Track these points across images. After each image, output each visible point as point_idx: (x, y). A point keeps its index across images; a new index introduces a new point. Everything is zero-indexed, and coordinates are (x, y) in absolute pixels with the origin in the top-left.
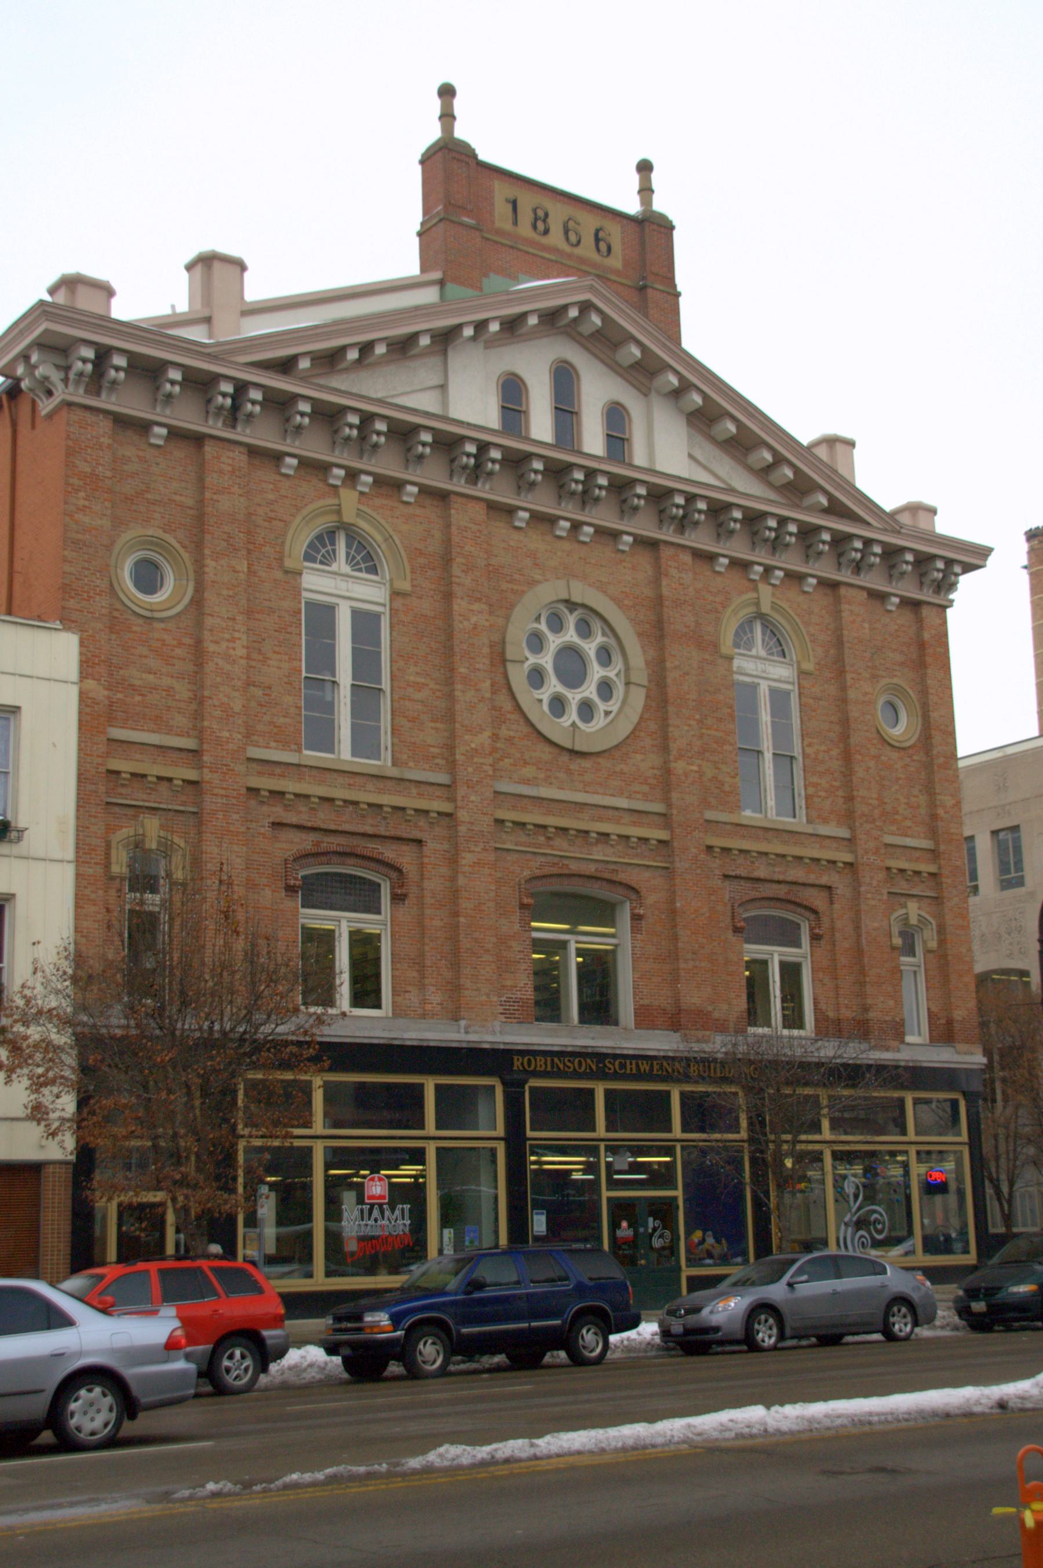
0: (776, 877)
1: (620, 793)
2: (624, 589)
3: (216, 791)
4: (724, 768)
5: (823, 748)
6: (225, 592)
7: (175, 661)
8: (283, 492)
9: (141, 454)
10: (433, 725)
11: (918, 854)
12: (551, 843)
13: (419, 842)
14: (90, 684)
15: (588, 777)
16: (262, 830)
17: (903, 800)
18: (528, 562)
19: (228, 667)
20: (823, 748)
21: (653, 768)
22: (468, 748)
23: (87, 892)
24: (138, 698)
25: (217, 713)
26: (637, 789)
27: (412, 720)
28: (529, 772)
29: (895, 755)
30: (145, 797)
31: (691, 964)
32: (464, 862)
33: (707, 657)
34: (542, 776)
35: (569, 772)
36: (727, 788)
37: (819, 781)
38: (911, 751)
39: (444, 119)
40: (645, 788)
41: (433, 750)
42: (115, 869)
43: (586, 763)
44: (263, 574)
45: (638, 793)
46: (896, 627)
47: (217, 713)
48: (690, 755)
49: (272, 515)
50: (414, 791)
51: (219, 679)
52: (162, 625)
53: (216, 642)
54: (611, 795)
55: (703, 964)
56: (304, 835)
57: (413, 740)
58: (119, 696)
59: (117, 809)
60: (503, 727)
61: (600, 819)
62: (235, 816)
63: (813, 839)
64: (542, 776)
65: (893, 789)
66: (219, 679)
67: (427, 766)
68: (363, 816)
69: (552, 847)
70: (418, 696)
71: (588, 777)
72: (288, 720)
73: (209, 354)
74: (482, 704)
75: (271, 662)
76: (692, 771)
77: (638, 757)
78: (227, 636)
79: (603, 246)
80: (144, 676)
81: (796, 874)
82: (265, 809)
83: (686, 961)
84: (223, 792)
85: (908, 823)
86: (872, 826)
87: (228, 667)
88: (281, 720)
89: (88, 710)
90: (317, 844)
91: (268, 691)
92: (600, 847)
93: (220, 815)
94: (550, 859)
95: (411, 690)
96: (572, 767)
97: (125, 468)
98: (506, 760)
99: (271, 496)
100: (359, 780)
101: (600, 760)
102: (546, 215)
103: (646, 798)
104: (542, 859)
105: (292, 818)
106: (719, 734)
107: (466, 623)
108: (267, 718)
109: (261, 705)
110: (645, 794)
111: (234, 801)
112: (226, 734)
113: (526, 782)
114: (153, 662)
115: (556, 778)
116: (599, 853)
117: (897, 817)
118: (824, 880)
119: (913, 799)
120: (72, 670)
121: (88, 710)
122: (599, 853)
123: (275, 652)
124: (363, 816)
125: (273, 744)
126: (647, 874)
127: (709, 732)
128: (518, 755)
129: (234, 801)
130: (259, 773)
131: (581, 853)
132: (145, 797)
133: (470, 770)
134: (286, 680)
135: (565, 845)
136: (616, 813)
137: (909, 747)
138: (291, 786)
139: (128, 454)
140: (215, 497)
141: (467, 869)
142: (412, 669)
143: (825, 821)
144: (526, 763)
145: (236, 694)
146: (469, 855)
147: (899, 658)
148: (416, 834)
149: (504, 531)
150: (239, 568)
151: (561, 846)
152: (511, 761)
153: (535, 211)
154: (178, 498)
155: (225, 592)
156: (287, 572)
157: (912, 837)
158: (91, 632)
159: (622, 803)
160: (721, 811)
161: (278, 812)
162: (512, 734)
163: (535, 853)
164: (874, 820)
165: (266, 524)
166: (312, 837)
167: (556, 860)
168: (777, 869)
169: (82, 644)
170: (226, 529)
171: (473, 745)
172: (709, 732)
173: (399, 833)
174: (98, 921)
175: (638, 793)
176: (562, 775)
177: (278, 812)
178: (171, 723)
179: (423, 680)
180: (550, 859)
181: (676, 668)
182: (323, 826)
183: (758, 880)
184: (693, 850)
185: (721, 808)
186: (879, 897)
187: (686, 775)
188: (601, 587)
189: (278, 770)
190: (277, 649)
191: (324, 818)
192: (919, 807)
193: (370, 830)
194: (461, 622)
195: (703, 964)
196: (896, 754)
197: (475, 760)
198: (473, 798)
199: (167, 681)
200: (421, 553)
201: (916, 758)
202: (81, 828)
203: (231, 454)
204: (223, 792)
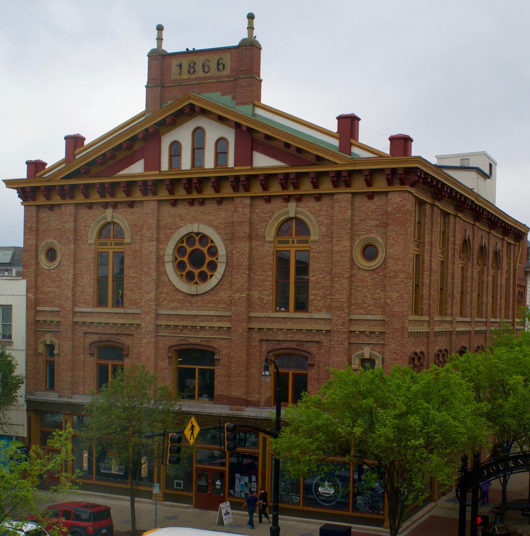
0: (288, 339)
1: (213, 309)
2: (221, 221)
3: (63, 324)
4: (265, 292)
5: (322, 276)
6: (67, 257)
7: (57, 282)
8: (90, 216)
9: (48, 214)
10: (138, 291)
11: (376, 323)
12: (182, 332)
13: (132, 335)
14: (30, 295)
15: (199, 304)
16: (81, 335)
17: (369, 296)
18: (178, 219)
19: (67, 283)
20: (322, 276)
21: (229, 297)
22: (146, 299)
23: (29, 359)
24: (47, 296)
25: (64, 299)
26: (221, 307)
27: (131, 291)
28: (174, 305)
29: (367, 274)
30: (48, 328)
31: (237, 379)
32: (143, 342)
33: (260, 243)
34: (179, 305)
35: (191, 303)
36: (265, 301)
37: (318, 292)
38: (378, 271)
39: (159, 40)
40: (225, 306)
41: (138, 301)
42: (40, 351)
43: (198, 298)
44: (82, 247)
45: (221, 308)
46: (376, 207)
47: (64, 299)
48: (242, 290)
49: (86, 225)
50: (131, 317)
51: (65, 287)
52: (53, 271)
53: (64, 275)
54: (209, 310)
55: (242, 379)
56: (96, 336)
57: (131, 298)
58: (41, 296)
59: (41, 332)
60: (165, 288)
61: (203, 321)
62: (69, 332)
63: (311, 320)
64: (179, 305)
65: (364, 292)
66: (65, 287)
67: (135, 307)
68: (113, 328)
69: (182, 333)
70: (133, 281)
71: (199, 304)
72: (89, 297)
73: (48, 180)
74: (152, 282)
75: (84, 277)
76: (242, 297)
77: (222, 293)
78: (67, 272)
79: (221, 67)
80: (48, 288)
81: (297, 337)
82: (82, 328)
83: (234, 377)
84: (65, 325)
85: (372, 308)
86: (342, 312)
87: (67, 283)
88: (87, 297)
89: (29, 303)
90: (100, 338)
91: (83, 288)
92: (202, 332)
93: (64, 332)
94: (181, 338)
95: (131, 279)
96: (192, 301)
97: (43, 221)
98: (166, 301)
99: (86, 218)
100: (112, 315)
101: (205, 296)
102: (195, 64)
103: (225, 310)
104: (179, 338)
105: (90, 330)
106: (264, 277)
107: (147, 251)
108: (83, 297)
109: (81, 293)
110: (224, 308)
111: (68, 327)
112: (66, 305)
113: (172, 309)
114: (50, 284)
115: (185, 306)
116: (202, 335)
117: (365, 305)
118: (316, 339)
119: (376, 295)
120: (24, 292)
121: (29, 303)
122: (202, 335)
123: (86, 274)
124: (113, 328)
125: (84, 306)
126: (223, 342)
127: (258, 277)
128: (170, 299)
129: (68, 327)
130: (80, 316)
131: (194, 335)
132: (48, 328)
133: (146, 308)
134: (89, 283)
135: (188, 332)
136: (211, 317)
137: (376, 269)
138: (88, 320)
139: (44, 216)
140: (64, 225)
141: (144, 345)
142: (132, 271)
143: (319, 311)
144: (173, 301)
145: (69, 291)
146: (144, 340)
147: (375, 223)
148: (131, 332)
149: (169, 209)
150: (71, 248)
151: (187, 334)
152: (168, 301)
153: (189, 65)
154: (58, 227)
155: (67, 257)
156: (90, 245)
157: (373, 314)
158: (30, 278)
159: (212, 313)
160: (262, 312)
161: (85, 329)
162: (168, 290)
163: (175, 336)
164: (343, 309)
165: (84, 229)
166: (99, 336)
167: (183, 338)
168: (289, 336)
169: (27, 282)
170: (67, 235)
171: (148, 298)
172: (258, 277)
173: (125, 333)
174: (389, 240)
175: (221, 308)
176: (188, 304)
177: (85, 329)
178: (55, 303)
179: (135, 275)
180: (181, 338)
181: (238, 252)
182: (100, 332)
183: (279, 341)
184: (241, 331)
185: (261, 310)
186: (343, 346)
187: (239, 299)
188: (210, 225)
189: (86, 315)
190: (86, 272)
191: (100, 330)
192: (380, 298)
193: (115, 332)
194: (145, 251)
195: (242, 379)
196: (368, 273)
197: (148, 304)
198: (147, 318)
199: (54, 289)
200: (136, 226)
201: (380, 274)
202: (27, 339)
203: (69, 208)
204: (65, 325)
